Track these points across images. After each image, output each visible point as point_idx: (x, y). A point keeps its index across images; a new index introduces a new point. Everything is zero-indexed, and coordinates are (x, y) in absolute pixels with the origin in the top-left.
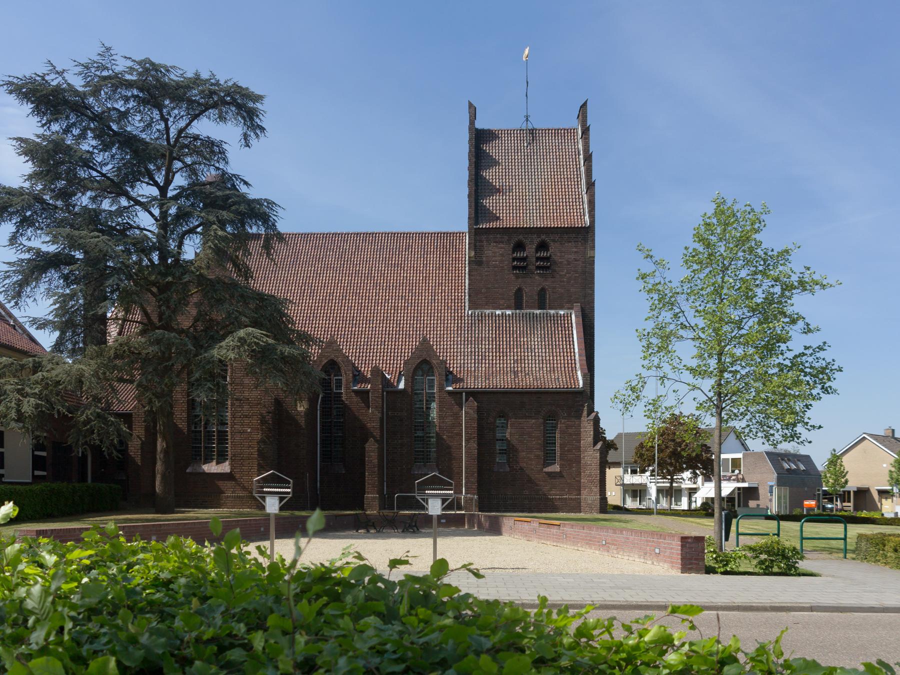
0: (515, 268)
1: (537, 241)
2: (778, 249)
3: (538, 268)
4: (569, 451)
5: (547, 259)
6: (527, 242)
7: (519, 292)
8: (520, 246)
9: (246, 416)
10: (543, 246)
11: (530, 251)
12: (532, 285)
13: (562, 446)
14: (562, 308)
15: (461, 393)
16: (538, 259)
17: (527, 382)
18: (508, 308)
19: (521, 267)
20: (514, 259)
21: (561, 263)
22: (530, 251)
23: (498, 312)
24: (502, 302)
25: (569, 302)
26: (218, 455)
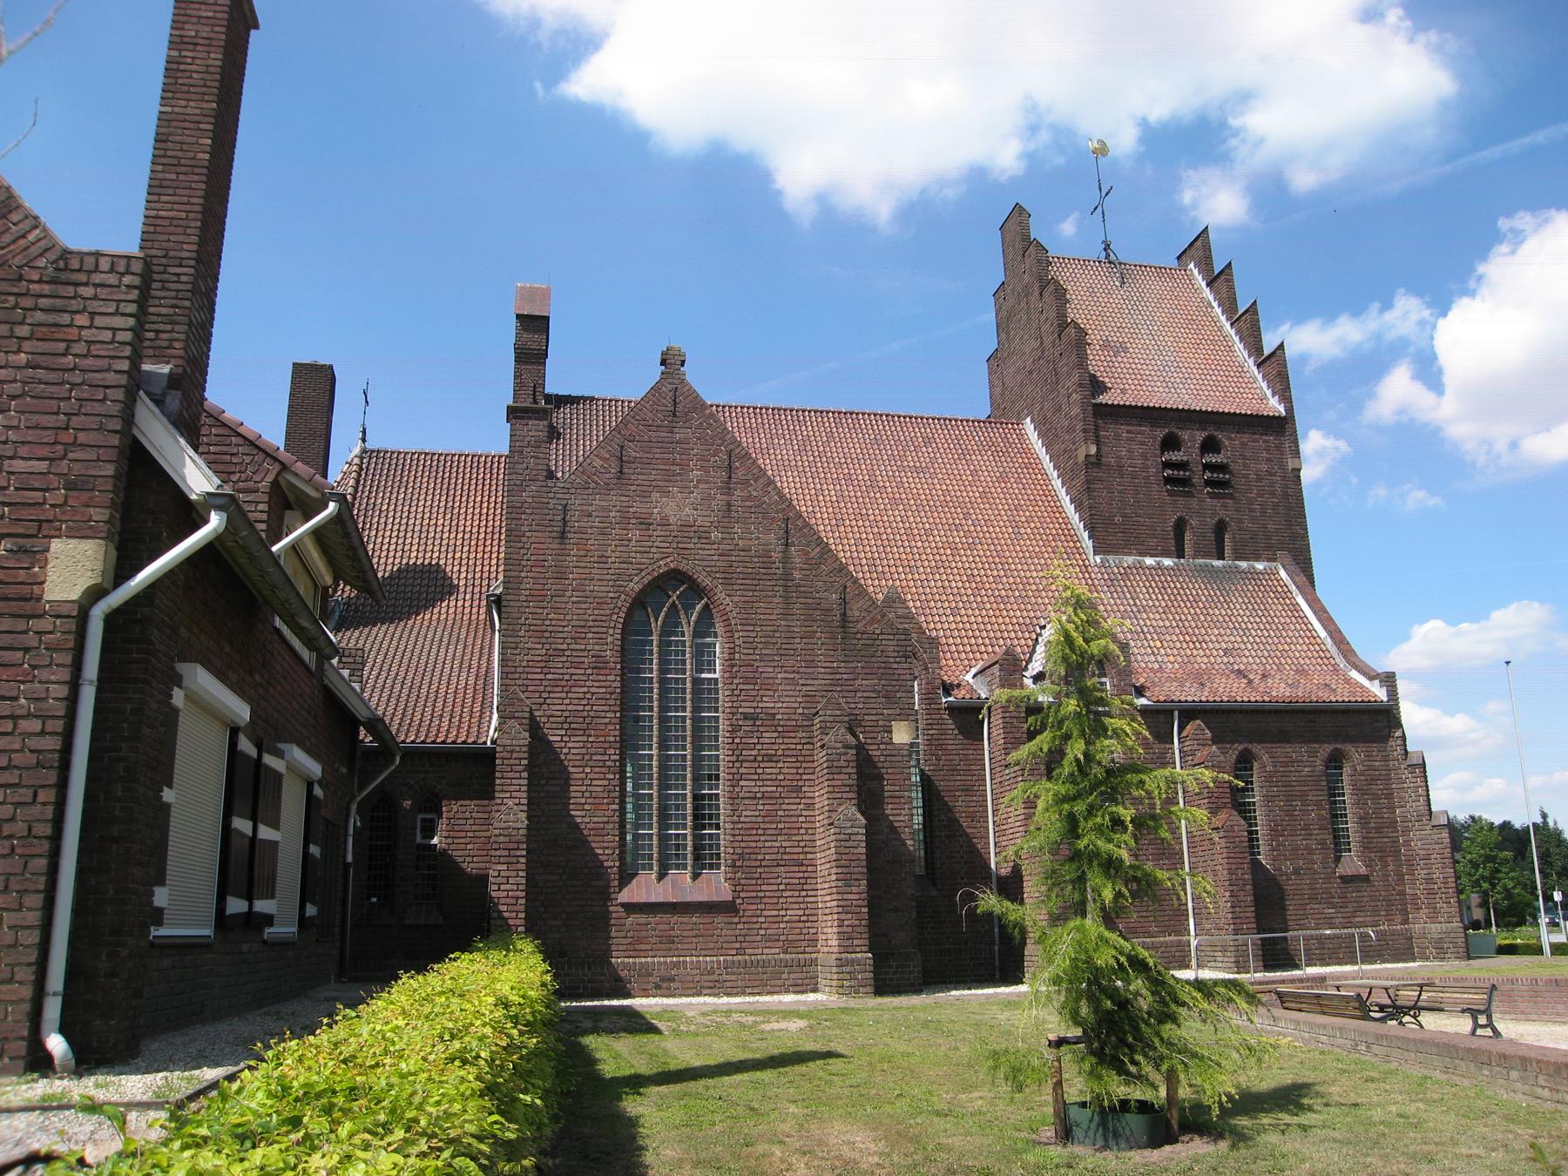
0: (1168, 480)
1: (1200, 436)
2: (655, 372)
3: (1208, 483)
4: (1378, 830)
5: (1221, 468)
6: (1185, 435)
7: (1180, 526)
8: (1170, 443)
9: (770, 758)
10: (1210, 446)
11: (1189, 452)
12: (1204, 509)
13: (1363, 820)
14: (1257, 559)
15: (1172, 712)
16: (1207, 467)
17: (635, 901)
18: (1167, 554)
19: (1177, 480)
20: (1167, 465)
21: (1245, 476)
22: (1189, 452)
23: (1149, 561)
24: (1152, 542)
25: (1268, 548)
26: (697, 857)
